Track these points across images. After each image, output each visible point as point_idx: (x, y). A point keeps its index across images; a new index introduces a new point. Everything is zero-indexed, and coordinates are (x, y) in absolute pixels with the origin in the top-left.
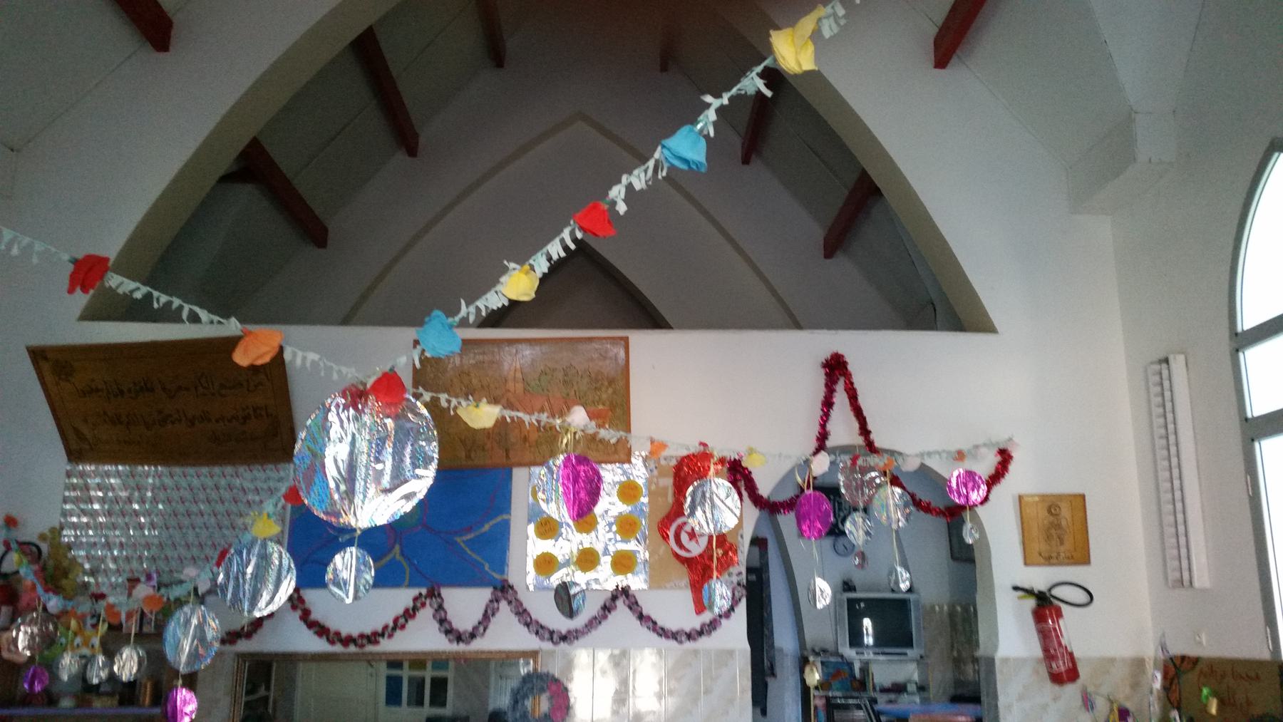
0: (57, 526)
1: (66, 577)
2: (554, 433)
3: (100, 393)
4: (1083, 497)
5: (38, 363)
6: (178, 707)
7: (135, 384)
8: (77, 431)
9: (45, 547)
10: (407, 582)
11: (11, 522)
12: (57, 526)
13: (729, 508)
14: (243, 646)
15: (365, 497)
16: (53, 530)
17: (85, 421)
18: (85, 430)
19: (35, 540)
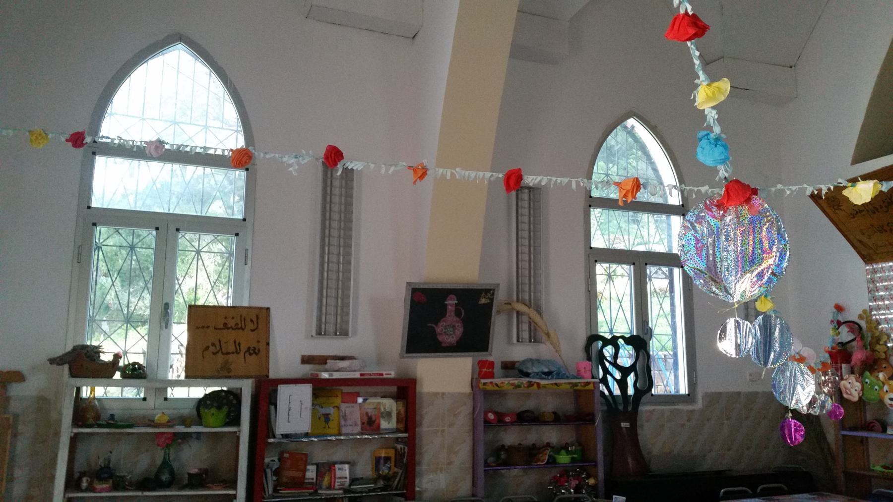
0: (868, 308)
1: (879, 344)
2: (698, 221)
3: (864, 213)
4: (268, 309)
5: (817, 202)
6: (338, 387)
7: (884, 202)
8: (860, 242)
9: (863, 324)
10: (488, 362)
11: (839, 308)
12: (868, 308)
13: (627, 320)
14: (575, 388)
15: (731, 295)
16: (865, 311)
17: (863, 234)
18: (865, 239)
19: (856, 319)
